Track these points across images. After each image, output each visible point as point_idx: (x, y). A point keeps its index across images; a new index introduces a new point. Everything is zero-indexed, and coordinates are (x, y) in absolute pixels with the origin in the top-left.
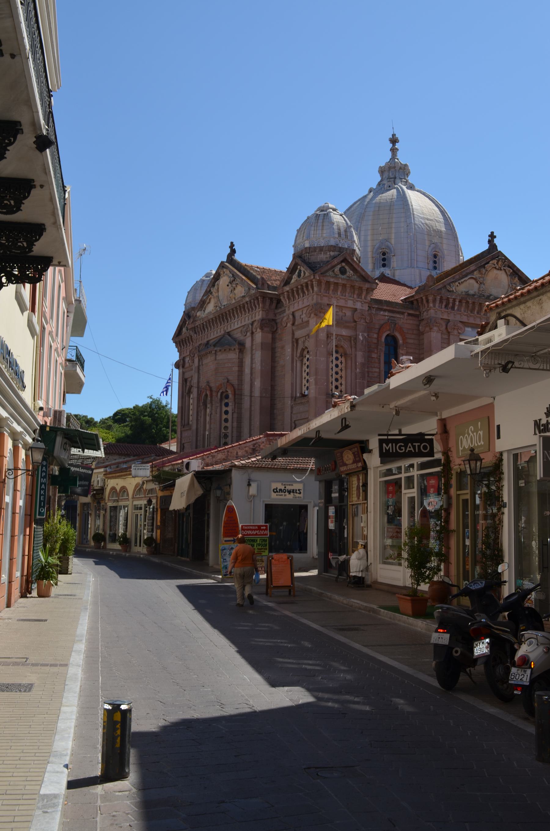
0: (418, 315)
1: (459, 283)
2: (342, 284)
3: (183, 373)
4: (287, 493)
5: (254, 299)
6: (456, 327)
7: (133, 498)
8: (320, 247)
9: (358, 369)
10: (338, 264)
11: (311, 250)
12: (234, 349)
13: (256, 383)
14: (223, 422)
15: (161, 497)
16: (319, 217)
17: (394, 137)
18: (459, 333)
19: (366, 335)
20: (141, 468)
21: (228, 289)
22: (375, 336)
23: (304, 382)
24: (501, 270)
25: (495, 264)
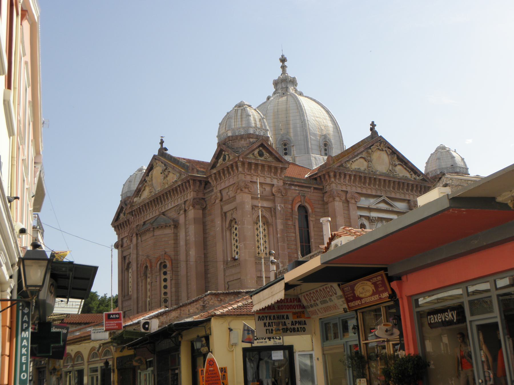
0: (322, 189)
1: (352, 162)
2: (261, 165)
3: (122, 252)
4: (267, 340)
5: (185, 183)
6: (353, 197)
7: (88, 362)
8: (241, 135)
9: (279, 235)
10: (256, 148)
11: (235, 138)
12: (170, 226)
13: (190, 253)
14: (162, 288)
15: (117, 358)
16: (237, 112)
17: (284, 57)
18: (356, 202)
19: (283, 206)
20: (100, 331)
21: (162, 177)
22: (290, 206)
23: (234, 248)
24: (383, 150)
25: (378, 145)
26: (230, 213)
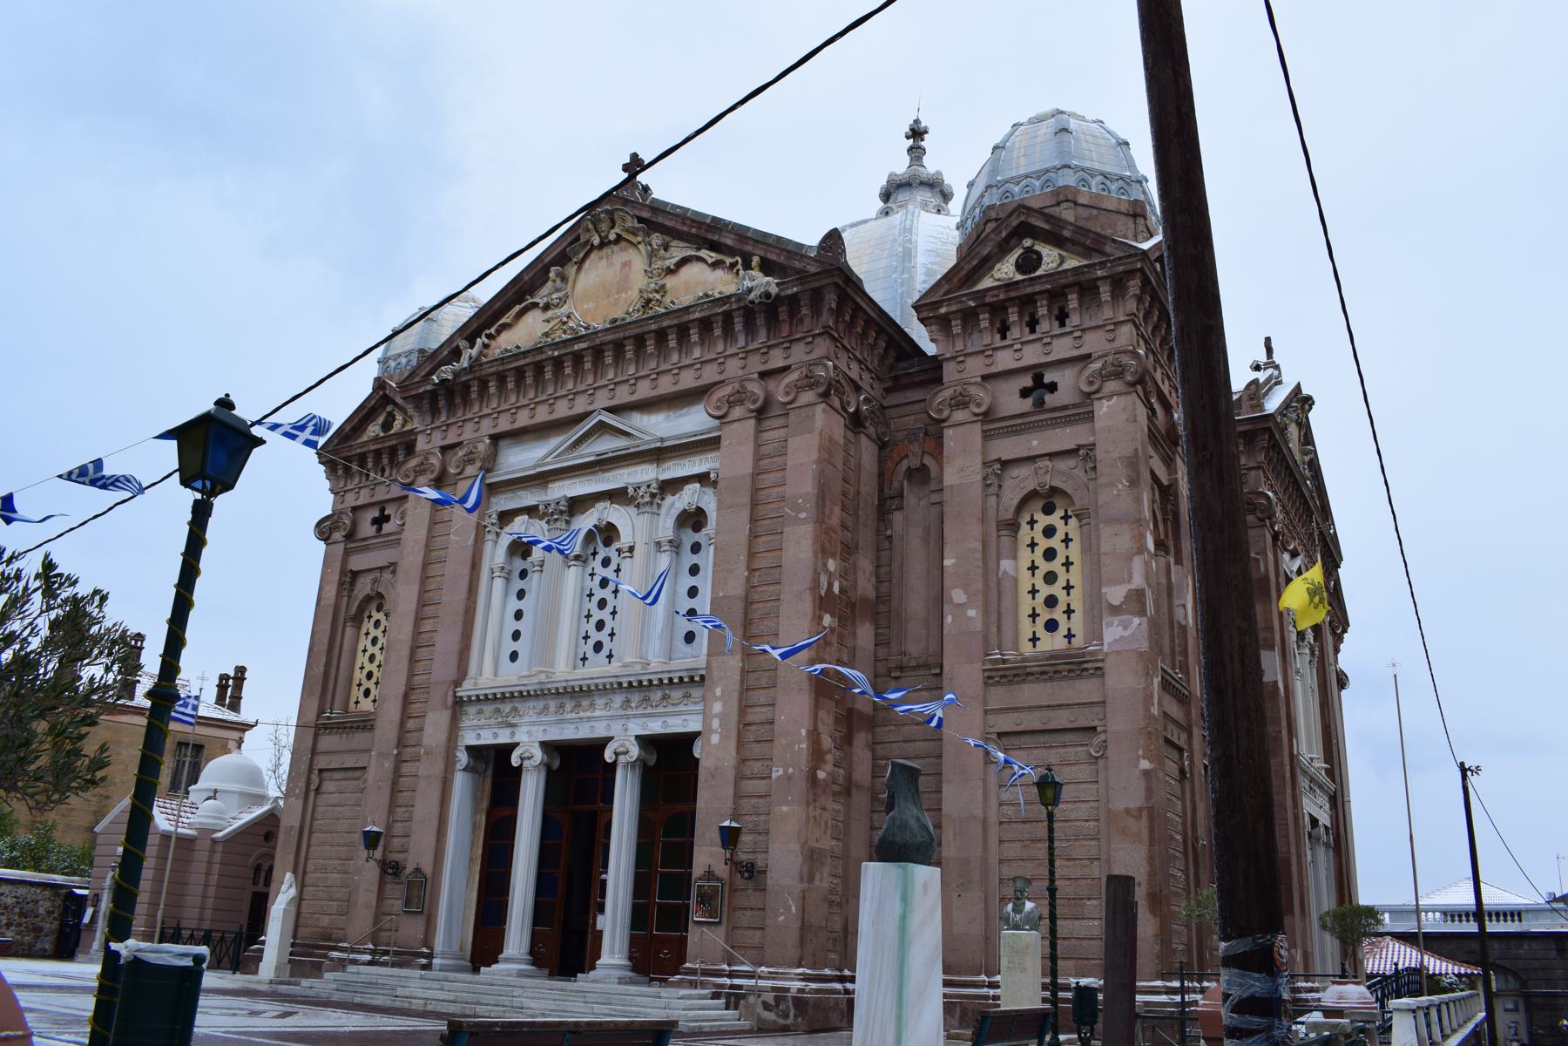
26: (371, 576)
